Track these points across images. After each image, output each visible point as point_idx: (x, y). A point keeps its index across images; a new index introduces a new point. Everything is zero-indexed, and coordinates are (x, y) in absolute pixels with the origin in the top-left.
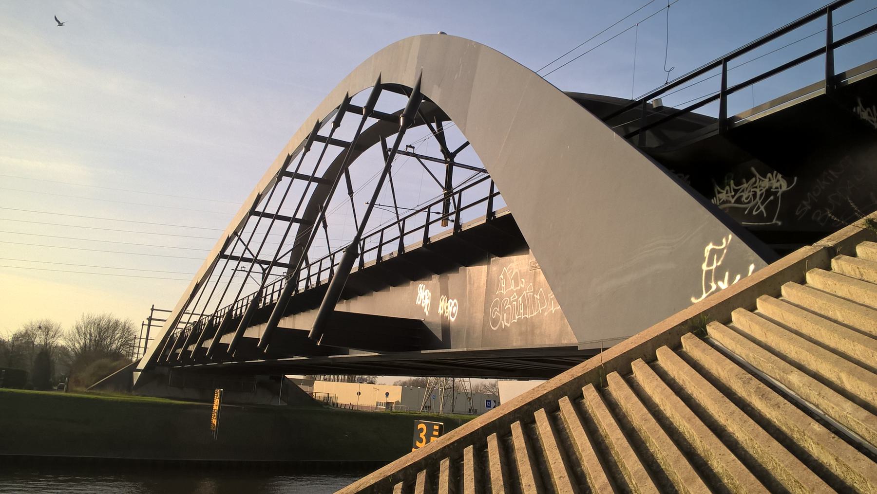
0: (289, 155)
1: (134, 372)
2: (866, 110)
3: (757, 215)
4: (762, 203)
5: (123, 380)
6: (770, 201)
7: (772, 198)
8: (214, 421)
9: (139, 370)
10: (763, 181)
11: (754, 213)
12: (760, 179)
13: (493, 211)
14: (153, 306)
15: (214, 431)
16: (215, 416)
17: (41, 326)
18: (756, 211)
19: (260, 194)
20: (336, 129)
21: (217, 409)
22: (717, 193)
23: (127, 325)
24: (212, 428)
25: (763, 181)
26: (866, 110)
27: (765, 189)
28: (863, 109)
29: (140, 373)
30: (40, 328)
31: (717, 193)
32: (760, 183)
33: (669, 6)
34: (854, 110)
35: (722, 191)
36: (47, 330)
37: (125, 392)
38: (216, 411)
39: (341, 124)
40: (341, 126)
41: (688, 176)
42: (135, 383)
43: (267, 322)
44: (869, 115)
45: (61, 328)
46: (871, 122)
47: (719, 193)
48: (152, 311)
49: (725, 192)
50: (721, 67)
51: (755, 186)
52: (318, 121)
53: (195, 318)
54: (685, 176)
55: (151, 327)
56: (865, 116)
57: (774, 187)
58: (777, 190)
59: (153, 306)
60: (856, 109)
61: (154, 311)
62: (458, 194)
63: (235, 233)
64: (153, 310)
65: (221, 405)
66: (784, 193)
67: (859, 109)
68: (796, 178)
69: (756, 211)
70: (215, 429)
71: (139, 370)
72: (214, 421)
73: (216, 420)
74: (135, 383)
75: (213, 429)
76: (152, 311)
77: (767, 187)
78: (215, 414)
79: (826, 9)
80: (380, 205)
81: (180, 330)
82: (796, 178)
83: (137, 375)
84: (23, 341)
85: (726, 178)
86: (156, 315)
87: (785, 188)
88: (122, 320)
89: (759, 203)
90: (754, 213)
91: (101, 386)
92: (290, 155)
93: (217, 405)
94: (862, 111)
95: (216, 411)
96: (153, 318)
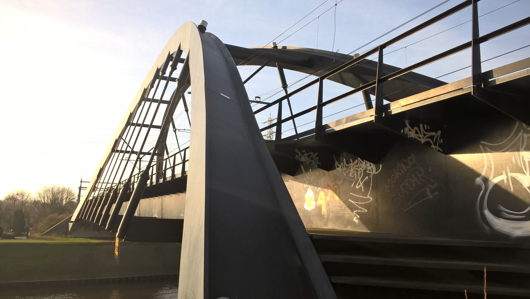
0: (145, 88)
1: (69, 223)
2: (413, 129)
3: (359, 188)
4: (362, 180)
5: (62, 230)
6: (365, 180)
7: (367, 178)
8: (117, 253)
9: (72, 222)
10: (362, 163)
11: (357, 187)
12: (360, 162)
13: (119, 214)
14: (82, 179)
15: (117, 259)
16: (116, 249)
17: (18, 193)
18: (358, 186)
19: (132, 113)
20: (173, 72)
21: (118, 245)
22: (336, 167)
23: (70, 190)
24: (115, 257)
25: (362, 163)
26: (413, 129)
27: (363, 169)
28: (411, 129)
29: (72, 224)
30: (18, 194)
31: (336, 167)
32: (360, 165)
33: (336, 5)
34: (402, 131)
35: (339, 166)
36: (22, 196)
37: (64, 236)
38: (117, 247)
39: (166, 72)
40: (177, 69)
41: (317, 154)
42: (70, 230)
43: (129, 200)
44: (416, 132)
45: (26, 195)
46: (419, 139)
47: (338, 167)
48: (81, 183)
49: (341, 166)
50: (278, 104)
51: (357, 166)
52: (158, 68)
53: (109, 185)
54: (314, 154)
55: (141, 162)
56: (412, 134)
57: (368, 170)
58: (370, 172)
59: (82, 179)
60: (404, 131)
61: (82, 183)
62: (184, 151)
63: (120, 137)
64: (81, 182)
65: (120, 241)
66: (374, 175)
67: (406, 130)
68: (381, 165)
69: (358, 186)
70: (117, 258)
71: (72, 222)
72: (117, 253)
73: (117, 252)
74: (70, 230)
75: (116, 258)
76: (81, 183)
77: (364, 169)
78: (117, 248)
79: (184, 149)
80: (184, 130)
81: (116, 184)
82: (381, 165)
83: (71, 225)
84: (12, 199)
85: (341, 156)
86: (83, 185)
87: (374, 172)
88: (67, 187)
89: (360, 181)
90: (357, 187)
91: (49, 233)
92: (146, 88)
93: (117, 243)
94: (410, 131)
95: (117, 247)
96: (82, 187)
